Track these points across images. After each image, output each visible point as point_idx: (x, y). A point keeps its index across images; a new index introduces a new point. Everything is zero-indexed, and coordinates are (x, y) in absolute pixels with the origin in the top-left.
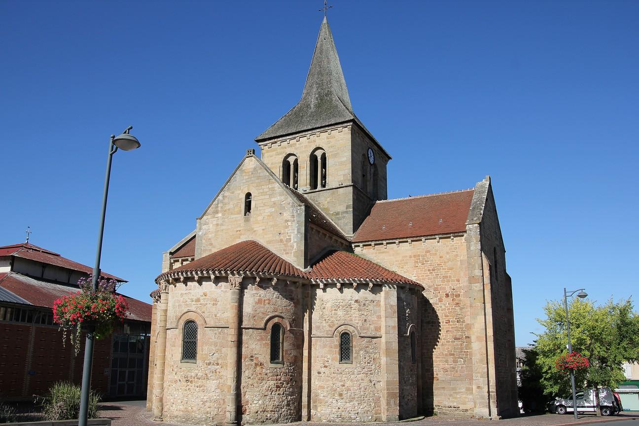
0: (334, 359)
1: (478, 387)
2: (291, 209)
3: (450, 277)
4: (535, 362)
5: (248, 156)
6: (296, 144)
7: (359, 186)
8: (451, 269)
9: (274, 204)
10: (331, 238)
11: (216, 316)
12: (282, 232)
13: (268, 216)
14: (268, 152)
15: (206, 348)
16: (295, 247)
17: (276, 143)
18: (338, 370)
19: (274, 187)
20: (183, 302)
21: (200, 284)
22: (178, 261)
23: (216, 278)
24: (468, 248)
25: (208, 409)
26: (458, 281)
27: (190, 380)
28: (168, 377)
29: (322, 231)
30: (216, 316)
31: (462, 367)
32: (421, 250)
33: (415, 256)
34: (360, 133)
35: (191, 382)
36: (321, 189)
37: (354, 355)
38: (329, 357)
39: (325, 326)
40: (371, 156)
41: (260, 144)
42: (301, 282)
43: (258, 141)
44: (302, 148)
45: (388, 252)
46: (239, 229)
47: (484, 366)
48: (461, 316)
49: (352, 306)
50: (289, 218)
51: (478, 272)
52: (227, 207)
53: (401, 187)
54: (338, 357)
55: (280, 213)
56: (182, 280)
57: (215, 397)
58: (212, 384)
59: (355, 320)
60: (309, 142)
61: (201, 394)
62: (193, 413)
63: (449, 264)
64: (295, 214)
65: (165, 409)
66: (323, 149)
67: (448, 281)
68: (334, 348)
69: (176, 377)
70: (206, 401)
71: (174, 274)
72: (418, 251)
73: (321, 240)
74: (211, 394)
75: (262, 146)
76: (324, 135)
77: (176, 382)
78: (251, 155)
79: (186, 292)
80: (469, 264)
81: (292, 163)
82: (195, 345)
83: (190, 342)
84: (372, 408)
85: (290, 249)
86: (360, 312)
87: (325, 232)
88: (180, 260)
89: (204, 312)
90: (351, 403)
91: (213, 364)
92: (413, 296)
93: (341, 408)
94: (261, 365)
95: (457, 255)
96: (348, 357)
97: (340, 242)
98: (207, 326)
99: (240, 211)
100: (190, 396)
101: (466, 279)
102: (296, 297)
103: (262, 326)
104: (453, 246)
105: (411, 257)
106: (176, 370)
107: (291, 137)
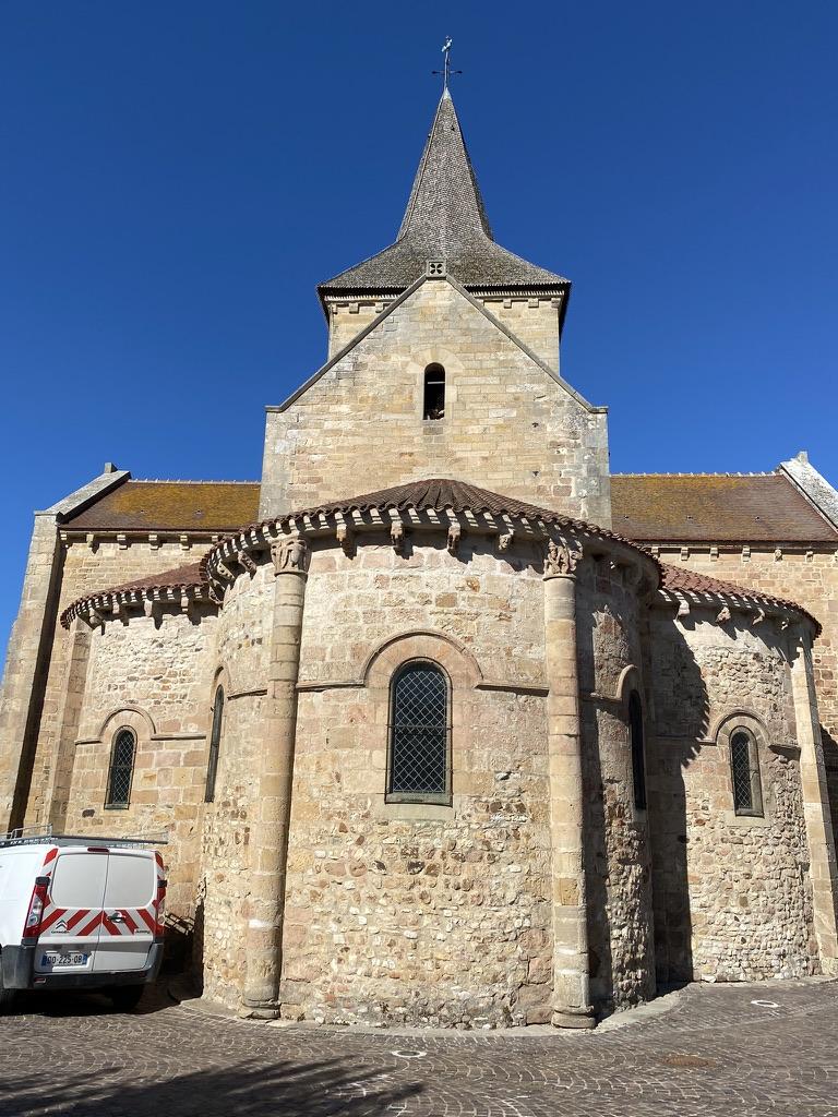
0: (721, 803)
9: (516, 399)
11: (509, 653)
12: (542, 470)
14: (347, 320)
18: (733, 833)
19: (513, 360)
20: (386, 603)
21: (351, 554)
22: (83, 539)
23: (408, 530)
25: (497, 967)
27: (428, 863)
30: (509, 653)
32: (737, 572)
35: (432, 871)
46: (408, 450)
49: (748, 667)
57: (517, 923)
58: (509, 874)
68: (719, 774)
71: (247, 535)
74: (503, 912)
75: (334, 306)
77: (359, 869)
82: (123, 786)
83: (425, 732)
88: (90, 537)
91: (508, 809)
93: (748, 940)
95: (820, 591)
98: (486, 682)
100: (426, 921)
104: (811, 569)
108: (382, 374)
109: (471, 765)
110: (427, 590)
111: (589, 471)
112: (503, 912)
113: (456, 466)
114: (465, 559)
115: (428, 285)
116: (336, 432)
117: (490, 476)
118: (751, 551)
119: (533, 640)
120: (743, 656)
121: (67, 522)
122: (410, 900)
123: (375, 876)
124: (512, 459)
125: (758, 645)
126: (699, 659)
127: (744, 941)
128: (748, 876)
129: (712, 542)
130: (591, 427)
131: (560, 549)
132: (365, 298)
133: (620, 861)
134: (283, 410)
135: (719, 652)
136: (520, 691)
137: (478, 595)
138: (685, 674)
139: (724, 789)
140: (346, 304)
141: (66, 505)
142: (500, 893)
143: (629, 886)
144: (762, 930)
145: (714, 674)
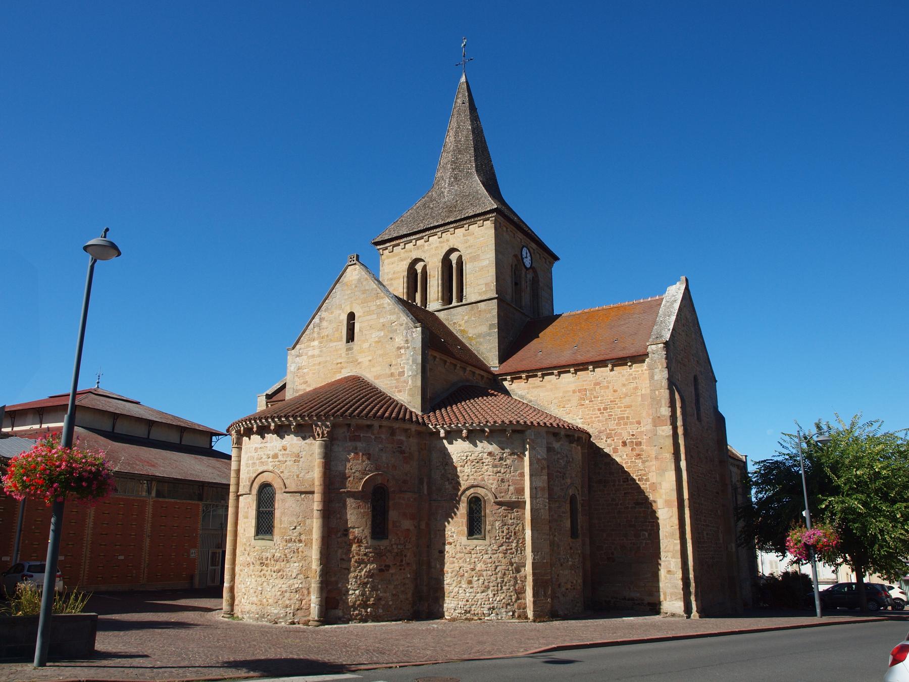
1: (669, 572)
2: (405, 332)
3: (628, 418)
4: (14, 594)
7: (508, 298)
8: (629, 407)
10: (464, 369)
11: (298, 476)
14: (388, 257)
16: (410, 382)
17: (398, 245)
20: (258, 459)
24: (652, 377)
25: (288, 602)
26: (639, 423)
28: (240, 559)
30: (298, 476)
33: (580, 391)
34: (509, 224)
35: (267, 565)
36: (457, 304)
37: (488, 527)
42: (413, 430)
43: (377, 244)
44: (431, 251)
45: (544, 386)
46: (339, 361)
48: (643, 472)
50: (403, 344)
51: (666, 411)
52: (324, 333)
54: (465, 529)
56: (255, 429)
57: (296, 586)
59: (489, 479)
63: (627, 401)
67: (626, 424)
69: (248, 559)
70: (286, 592)
73: (451, 373)
74: (291, 582)
79: (262, 445)
80: (653, 399)
81: (419, 271)
87: (454, 361)
89: (282, 472)
94: (358, 542)
98: (287, 490)
99: (342, 338)
100: (265, 584)
101: (650, 421)
103: (247, 491)
105: (574, 392)
106: (248, 549)
107: (417, 236)
112: (291, 582)
114: (282, 437)
116: (313, 356)
118: (594, 368)
124: (381, 359)
125: (493, 448)
126: (455, 458)
127: (467, 601)
128: (473, 570)
129: (569, 366)
132: (405, 239)
134: (293, 348)
136: (301, 493)
143: (363, 573)
144: (479, 596)
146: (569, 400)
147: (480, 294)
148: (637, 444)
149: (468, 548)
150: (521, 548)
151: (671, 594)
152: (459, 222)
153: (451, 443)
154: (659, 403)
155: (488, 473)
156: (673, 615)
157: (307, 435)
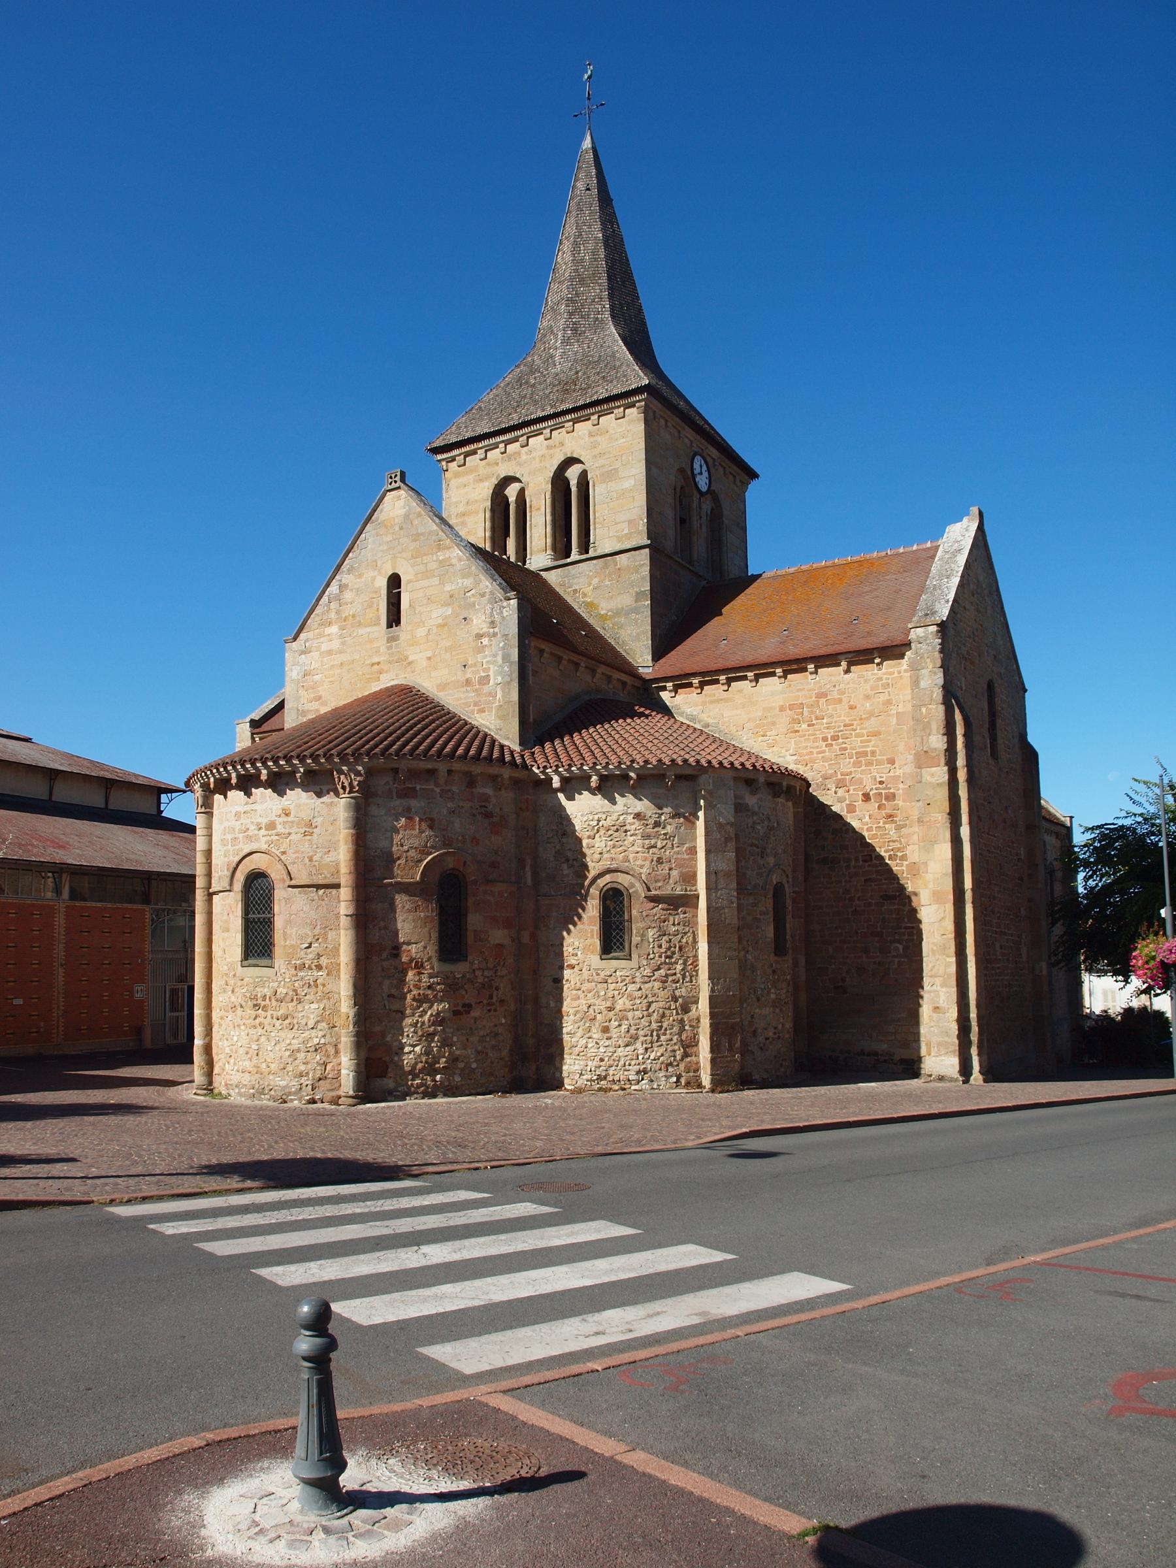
1: (936, 1009)
2: (488, 607)
3: (873, 753)
5: (390, 487)
6: (519, 454)
7: (669, 545)
8: (876, 734)
9: (451, 596)
11: (311, 860)
13: (438, 626)
14: (457, 475)
15: (294, 931)
16: (499, 695)
17: (474, 452)
18: (598, 974)
20: (241, 831)
24: (915, 683)
25: (302, 1068)
26: (892, 762)
27: (263, 1003)
29: (567, 656)
30: (311, 860)
31: (900, 963)
33: (791, 707)
35: (265, 1008)
36: (578, 558)
37: (636, 939)
38: (577, 943)
39: (568, 875)
40: (701, 473)
41: (439, 457)
42: (506, 776)
43: (436, 451)
44: (532, 463)
46: (376, 660)
47: (948, 960)
48: (897, 845)
49: (628, 827)
50: (485, 628)
51: (938, 742)
52: (348, 611)
53: (774, 539)
55: (465, 619)
57: (316, 1041)
58: (311, 1010)
59: (636, 859)
60: (548, 447)
61: (287, 1035)
62: (271, 1077)
63: (872, 724)
64: (497, 618)
65: (216, 1070)
66: (581, 462)
67: (869, 764)
68: (590, 925)
69: (233, 999)
70: (299, 1050)
72: (800, 693)
74: (306, 1034)
75: (444, 463)
76: (583, 428)
78: (397, 485)
79: (248, 808)
84: (678, 1058)
85: (489, 705)
86: (647, 842)
87: (575, 658)
89: (284, 853)
90: (628, 1048)
92: (780, 800)
96: (621, 944)
97: (619, 680)
99: (378, 618)
100: (263, 1039)
101: (911, 758)
102: (498, 810)
104: (881, 679)
105: (782, 709)
108: (358, 591)
109: (285, 940)
110: (260, 820)
111: (503, 659)
112: (306, 1034)
113: (409, 669)
114: (281, 793)
115: (389, 496)
116: (330, 652)
117: (433, 674)
118: (817, 668)
119: (330, 847)
120: (622, 818)
121: (260, 726)
122: (255, 1027)
123: (239, 1011)
124: (448, 656)
125: (643, 806)
126: (578, 824)
128: (610, 1009)
130: (505, 614)
131: (342, 777)
132: (487, 442)
133: (414, 999)
134: (295, 639)
135: (596, 817)
136: (318, 887)
137: (290, 819)
138: (564, 840)
139: (592, 936)
140: (453, 459)
141: (257, 715)
142: (303, 1022)
143: (426, 1018)
145: (589, 837)
146: (774, 724)
147: (619, 539)
148: (887, 798)
149: (602, 974)
150: (690, 972)
151: (939, 1044)
152: (581, 412)
153: (571, 798)
154: (926, 727)
155: (636, 848)
156: (941, 1078)
157: (325, 788)
